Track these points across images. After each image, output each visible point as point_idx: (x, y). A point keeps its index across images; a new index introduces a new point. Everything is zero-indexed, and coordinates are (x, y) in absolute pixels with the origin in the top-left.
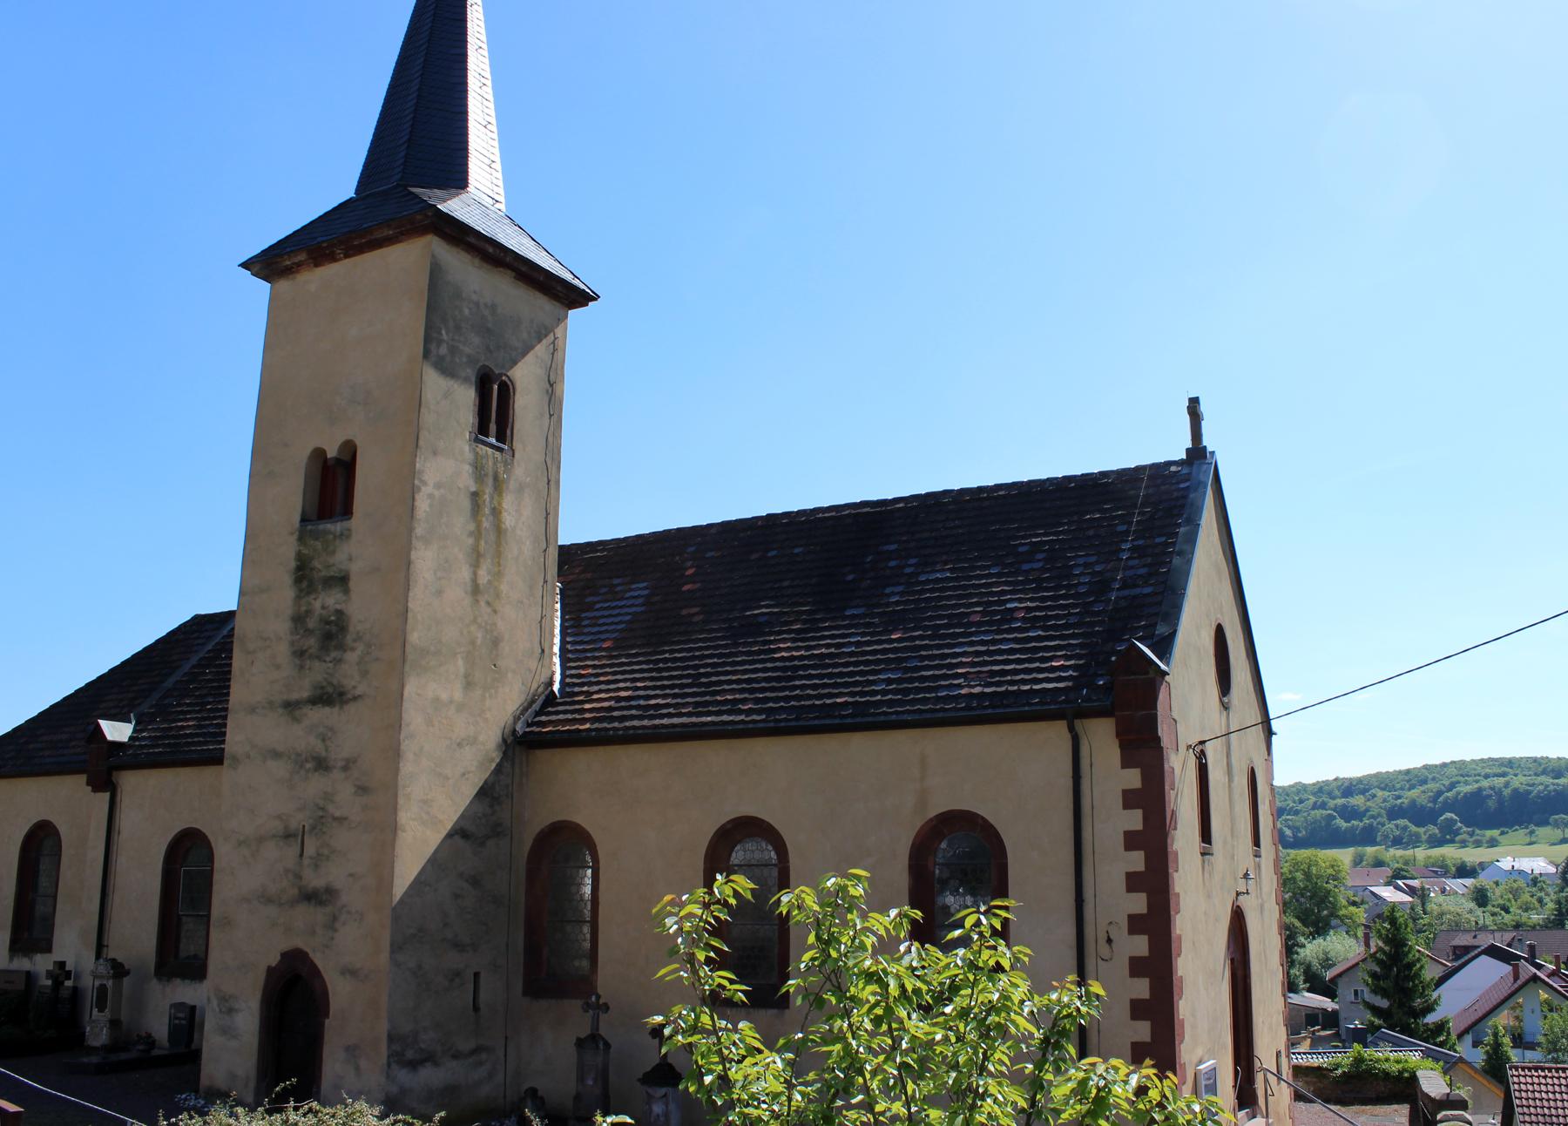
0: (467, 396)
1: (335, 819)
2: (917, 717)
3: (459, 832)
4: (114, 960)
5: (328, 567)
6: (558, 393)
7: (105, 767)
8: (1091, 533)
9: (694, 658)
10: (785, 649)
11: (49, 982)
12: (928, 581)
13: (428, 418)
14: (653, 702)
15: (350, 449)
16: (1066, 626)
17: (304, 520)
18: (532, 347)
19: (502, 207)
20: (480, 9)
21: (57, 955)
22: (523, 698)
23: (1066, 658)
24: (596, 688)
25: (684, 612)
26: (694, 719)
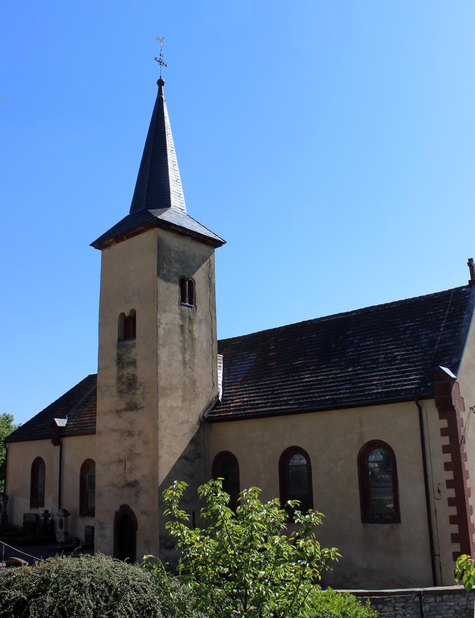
0: (175, 289)
1: (136, 454)
2: (356, 403)
3: (184, 457)
4: (64, 510)
5: (129, 358)
6: (213, 282)
7: (58, 436)
8: (429, 320)
9: (272, 383)
10: (307, 378)
11: (43, 518)
12: (364, 346)
13: (161, 298)
14: (256, 402)
15: (133, 312)
16: (417, 361)
17: (119, 340)
18: (201, 266)
19: (185, 211)
20: (171, 136)
21: (46, 508)
22: (207, 403)
23: (416, 375)
24: (235, 398)
25: (269, 364)
26: (271, 409)
